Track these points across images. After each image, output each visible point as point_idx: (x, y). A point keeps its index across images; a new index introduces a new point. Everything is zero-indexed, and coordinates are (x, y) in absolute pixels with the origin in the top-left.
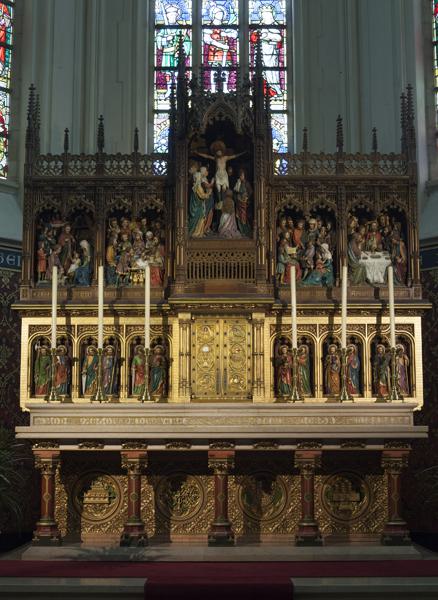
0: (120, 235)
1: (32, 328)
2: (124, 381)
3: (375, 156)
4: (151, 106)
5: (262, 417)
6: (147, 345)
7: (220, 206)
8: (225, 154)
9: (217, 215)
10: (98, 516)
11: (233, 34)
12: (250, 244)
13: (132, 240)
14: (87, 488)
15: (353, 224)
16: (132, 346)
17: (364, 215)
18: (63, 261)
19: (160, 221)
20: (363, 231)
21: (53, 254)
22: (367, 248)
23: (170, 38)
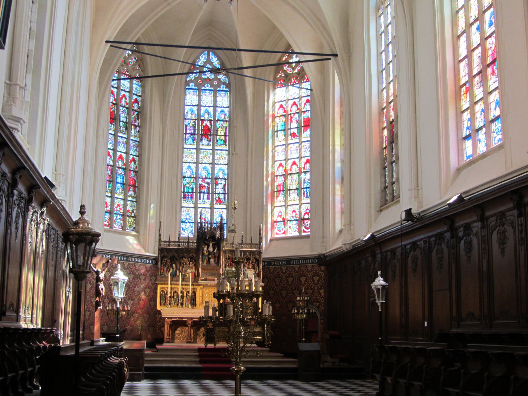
0: (183, 263)
1: (160, 288)
2: (184, 302)
3: (251, 244)
4: (181, 205)
5: (134, 262)
6: (9, 175)
7: (210, 256)
8: (212, 242)
9: (209, 259)
10: (179, 337)
11: (209, 181)
12: (218, 267)
13: (186, 264)
14: (176, 330)
15: (245, 262)
16: (187, 293)
17: (248, 260)
18: (168, 270)
19: (195, 260)
20: (248, 263)
21: (165, 268)
22: (248, 268)
23: (188, 181)
